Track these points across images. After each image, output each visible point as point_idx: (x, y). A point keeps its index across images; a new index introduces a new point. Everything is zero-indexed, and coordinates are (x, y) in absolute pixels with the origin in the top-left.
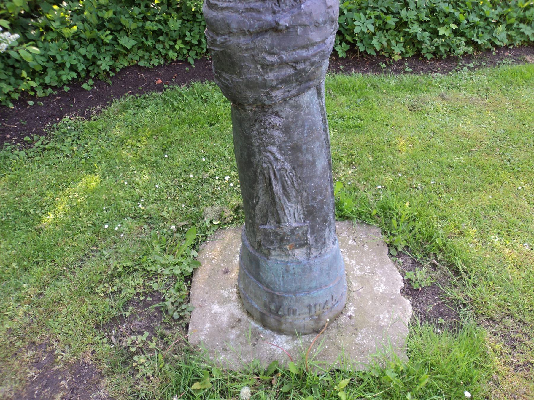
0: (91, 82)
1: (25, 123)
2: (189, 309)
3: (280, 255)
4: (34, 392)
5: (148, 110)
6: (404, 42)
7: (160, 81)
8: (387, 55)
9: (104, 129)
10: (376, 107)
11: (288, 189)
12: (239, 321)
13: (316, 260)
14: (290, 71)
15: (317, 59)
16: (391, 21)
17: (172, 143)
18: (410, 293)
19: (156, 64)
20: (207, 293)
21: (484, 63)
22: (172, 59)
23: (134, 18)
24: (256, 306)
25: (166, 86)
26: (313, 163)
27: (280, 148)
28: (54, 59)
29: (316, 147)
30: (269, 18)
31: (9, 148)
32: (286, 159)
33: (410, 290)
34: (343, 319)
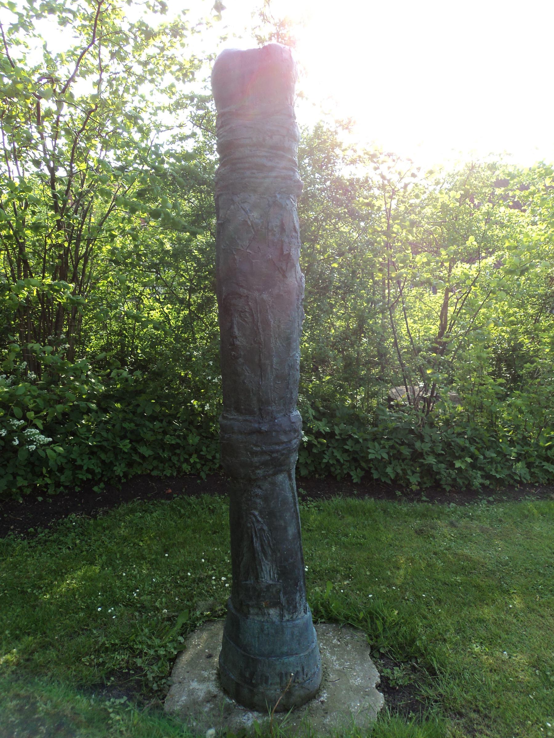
0: (102, 485)
1: (31, 516)
2: (169, 683)
3: (257, 614)
4: (13, 733)
5: (154, 515)
6: (421, 473)
7: (170, 491)
8: (404, 485)
9: (108, 528)
10: (382, 528)
11: (265, 547)
12: (215, 696)
13: (288, 623)
14: (268, 457)
15: (285, 452)
16: (406, 451)
17: (174, 544)
18: (386, 690)
19: (168, 475)
20: (188, 672)
21: (505, 498)
22: (185, 472)
23: (154, 431)
24: (233, 677)
25: (175, 495)
26: (285, 529)
27: (261, 513)
28: (74, 460)
29: (288, 516)
30: (257, 425)
31: (12, 537)
32: (264, 522)
33: (385, 686)
34: (315, 703)
